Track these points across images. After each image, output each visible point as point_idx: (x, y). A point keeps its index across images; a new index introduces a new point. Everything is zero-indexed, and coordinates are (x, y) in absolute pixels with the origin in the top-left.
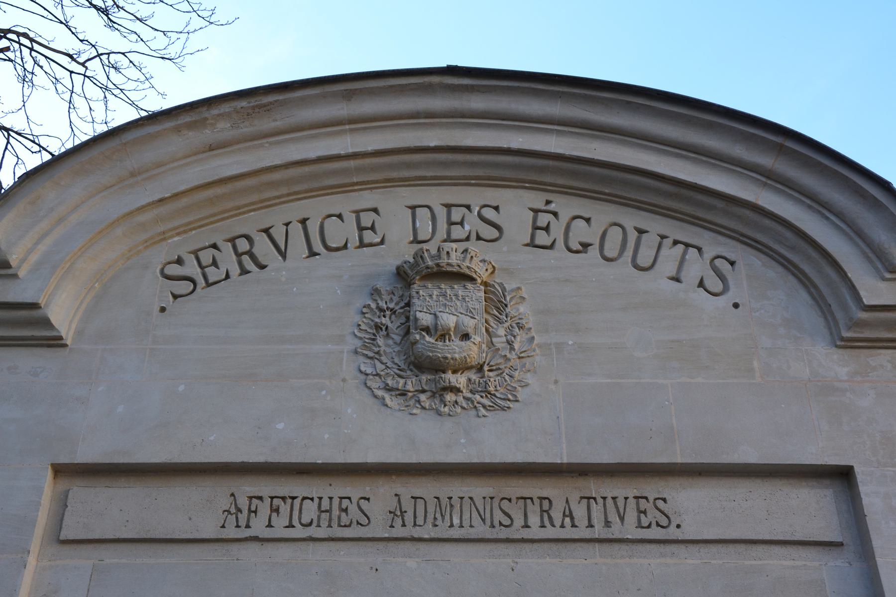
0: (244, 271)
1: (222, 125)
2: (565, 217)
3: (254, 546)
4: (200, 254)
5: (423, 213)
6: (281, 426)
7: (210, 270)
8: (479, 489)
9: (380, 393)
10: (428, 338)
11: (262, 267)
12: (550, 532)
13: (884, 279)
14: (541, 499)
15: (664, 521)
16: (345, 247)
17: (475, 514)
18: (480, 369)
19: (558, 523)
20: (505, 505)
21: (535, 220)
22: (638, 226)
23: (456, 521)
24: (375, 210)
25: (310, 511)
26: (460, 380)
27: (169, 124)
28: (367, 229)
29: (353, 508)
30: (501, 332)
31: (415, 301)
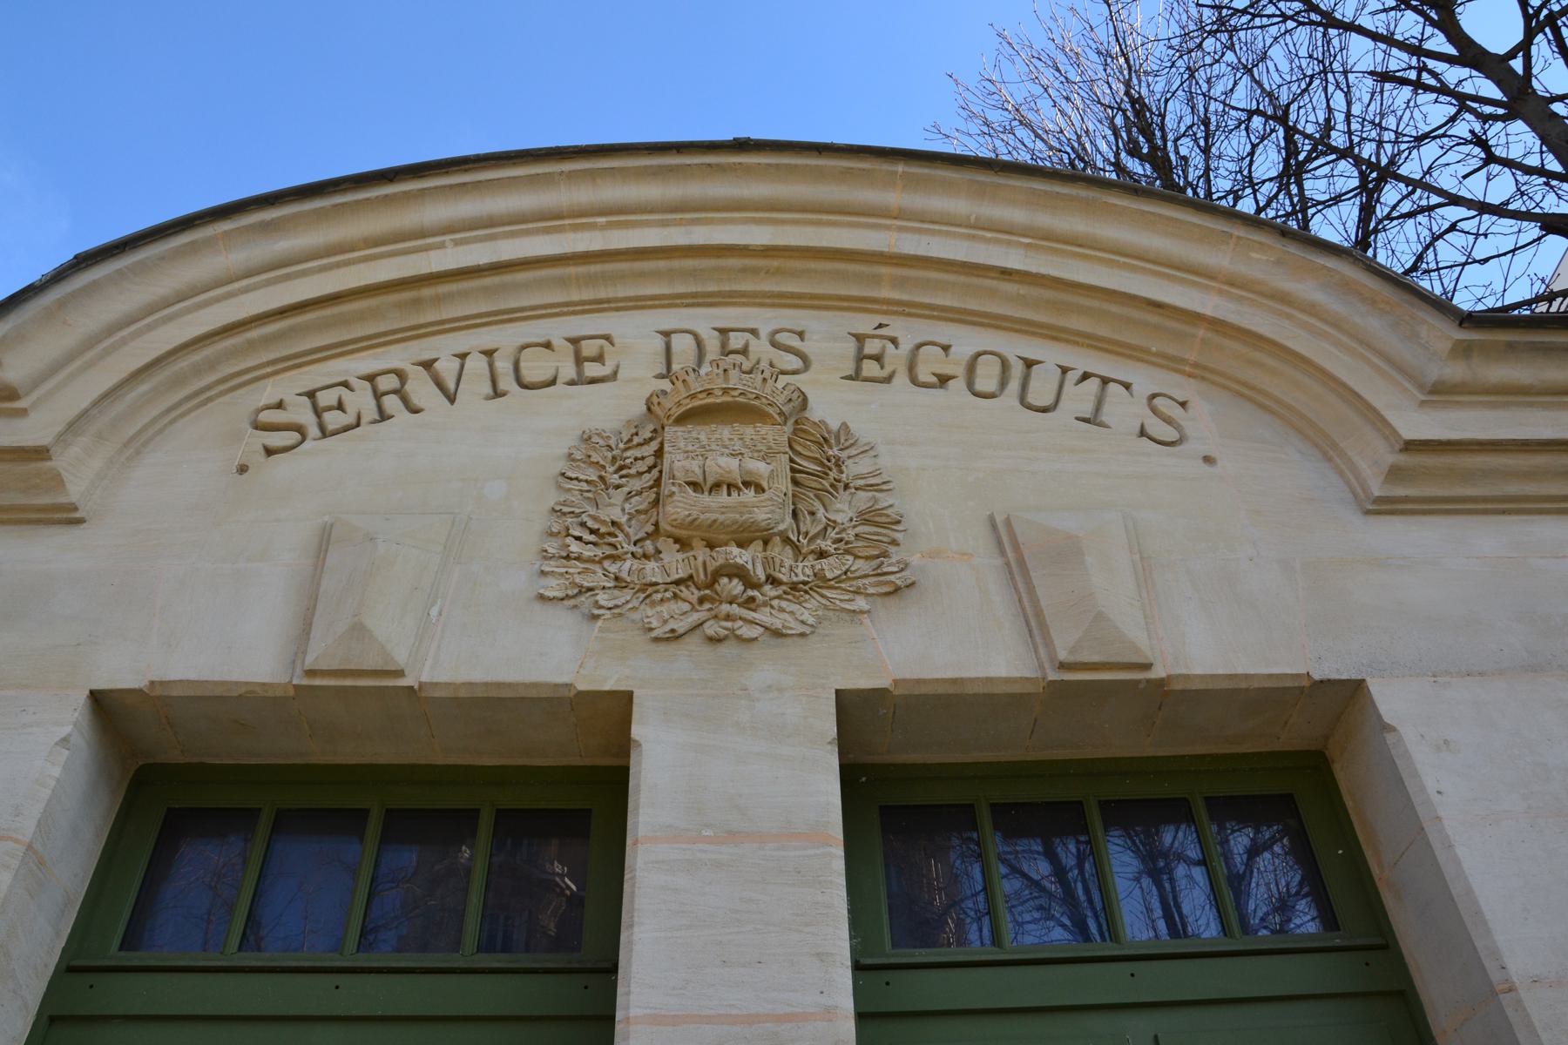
0: (383, 416)
2: (906, 346)
21: (860, 349)
22: (939, 371)
24: (607, 338)
28: (330, 409)
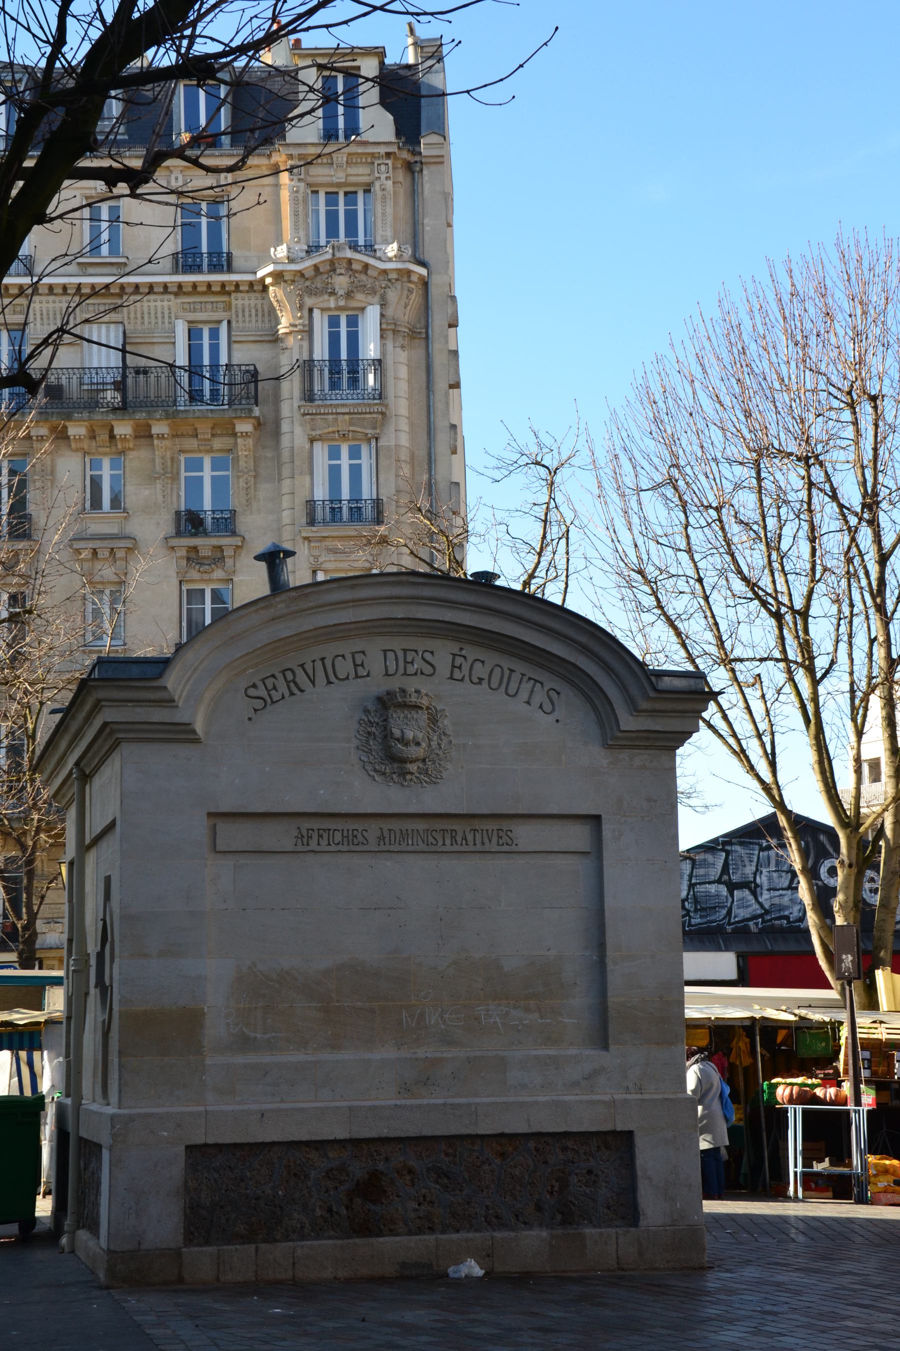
0: (292, 694)
1: (281, 606)
2: (470, 659)
3: (312, 855)
4: (266, 681)
5: (390, 655)
6: (322, 792)
7: (273, 692)
8: (421, 825)
9: (372, 773)
10: (399, 746)
11: (302, 691)
12: (455, 848)
13: (632, 715)
14: (452, 830)
15: (510, 842)
16: (347, 678)
17: (419, 839)
18: (424, 760)
19: (459, 843)
20: (434, 833)
23: (410, 842)
25: (338, 837)
26: (413, 767)
27: (252, 609)
29: (359, 835)
30: (435, 738)
31: (390, 720)
